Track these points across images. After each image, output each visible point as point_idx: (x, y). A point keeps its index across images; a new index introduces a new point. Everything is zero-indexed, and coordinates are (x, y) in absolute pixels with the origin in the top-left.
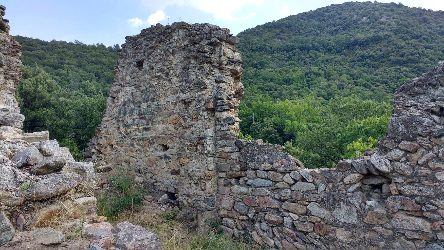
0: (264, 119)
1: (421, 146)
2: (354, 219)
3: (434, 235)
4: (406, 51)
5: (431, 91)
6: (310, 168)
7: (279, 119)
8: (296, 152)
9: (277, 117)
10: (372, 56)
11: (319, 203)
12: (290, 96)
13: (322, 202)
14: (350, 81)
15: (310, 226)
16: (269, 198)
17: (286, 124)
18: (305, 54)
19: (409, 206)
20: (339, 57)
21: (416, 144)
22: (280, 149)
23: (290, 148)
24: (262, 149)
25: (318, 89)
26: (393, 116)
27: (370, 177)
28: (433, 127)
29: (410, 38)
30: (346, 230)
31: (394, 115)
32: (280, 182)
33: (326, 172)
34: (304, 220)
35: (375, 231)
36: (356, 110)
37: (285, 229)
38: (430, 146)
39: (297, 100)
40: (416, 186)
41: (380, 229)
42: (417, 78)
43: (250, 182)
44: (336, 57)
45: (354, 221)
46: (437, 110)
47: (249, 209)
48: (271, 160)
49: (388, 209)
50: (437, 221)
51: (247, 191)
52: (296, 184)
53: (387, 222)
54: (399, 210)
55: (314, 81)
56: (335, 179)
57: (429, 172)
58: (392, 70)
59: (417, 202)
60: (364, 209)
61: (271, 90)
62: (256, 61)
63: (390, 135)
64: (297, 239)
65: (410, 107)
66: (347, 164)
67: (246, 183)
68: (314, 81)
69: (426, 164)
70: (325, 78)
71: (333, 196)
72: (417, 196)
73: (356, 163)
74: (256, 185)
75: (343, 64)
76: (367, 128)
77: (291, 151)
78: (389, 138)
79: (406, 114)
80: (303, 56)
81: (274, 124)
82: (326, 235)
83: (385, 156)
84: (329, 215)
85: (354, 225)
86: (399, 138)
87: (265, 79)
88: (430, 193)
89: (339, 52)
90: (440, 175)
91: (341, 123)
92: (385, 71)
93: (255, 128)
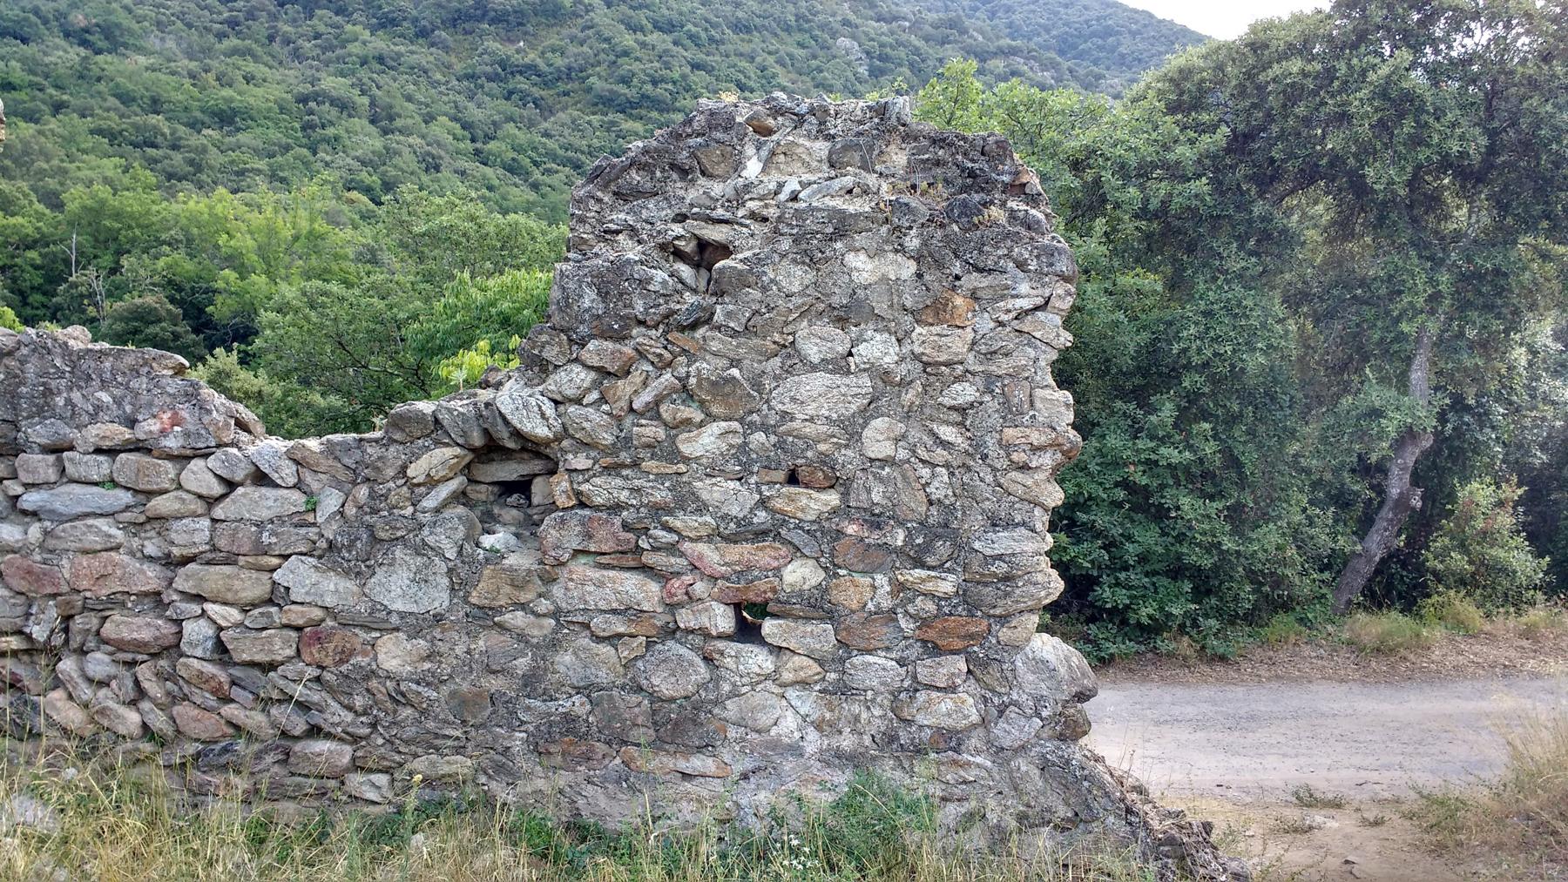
0: (124, 262)
1: (641, 354)
2: (438, 598)
3: (669, 618)
4: (636, 66)
5: (676, 187)
6: (289, 435)
7: (189, 266)
8: (256, 389)
9: (179, 256)
10: (531, 69)
11: (320, 557)
12: (238, 179)
13: (328, 554)
14: (461, 146)
15: (286, 642)
16: (120, 557)
17: (220, 284)
18: (295, 20)
19: (604, 540)
20: (422, 55)
21: (628, 350)
22: (166, 367)
23: (228, 375)
24: (87, 364)
25: (349, 160)
26: (567, 260)
27: (494, 456)
28: (677, 297)
29: (650, 26)
30: (410, 637)
31: (571, 255)
32: (166, 492)
33: (346, 447)
34: (262, 622)
35: (502, 627)
36: (474, 243)
37: (185, 664)
38: (667, 355)
39: (263, 191)
40: (626, 478)
41: (517, 619)
42: (640, 144)
43: (31, 500)
44: (412, 53)
45: (436, 604)
46: (688, 247)
47: (30, 606)
48: (128, 409)
49: (545, 553)
50: (678, 574)
51: (19, 536)
52: (232, 496)
53: (540, 596)
54: (577, 553)
55: (330, 131)
56: (377, 469)
57: (661, 433)
58: (596, 124)
59: (626, 527)
60: (470, 562)
61: (154, 146)
62: (86, 16)
63: (556, 319)
64: (236, 692)
65: (618, 232)
66: (420, 418)
67: (14, 506)
68: (330, 131)
69: (653, 411)
70: (372, 122)
71: (370, 528)
72: (627, 506)
73: (450, 411)
74: (62, 509)
75: (439, 83)
76: (505, 306)
77: (236, 385)
78: (553, 328)
79: (604, 254)
80: (287, 28)
81: (170, 282)
82: (342, 662)
83: (540, 388)
84: (353, 594)
85: (438, 618)
86: (583, 329)
87: (126, 98)
88: (661, 495)
89: (423, 33)
90: (688, 440)
91: (422, 286)
92: (575, 126)
93: (82, 296)
